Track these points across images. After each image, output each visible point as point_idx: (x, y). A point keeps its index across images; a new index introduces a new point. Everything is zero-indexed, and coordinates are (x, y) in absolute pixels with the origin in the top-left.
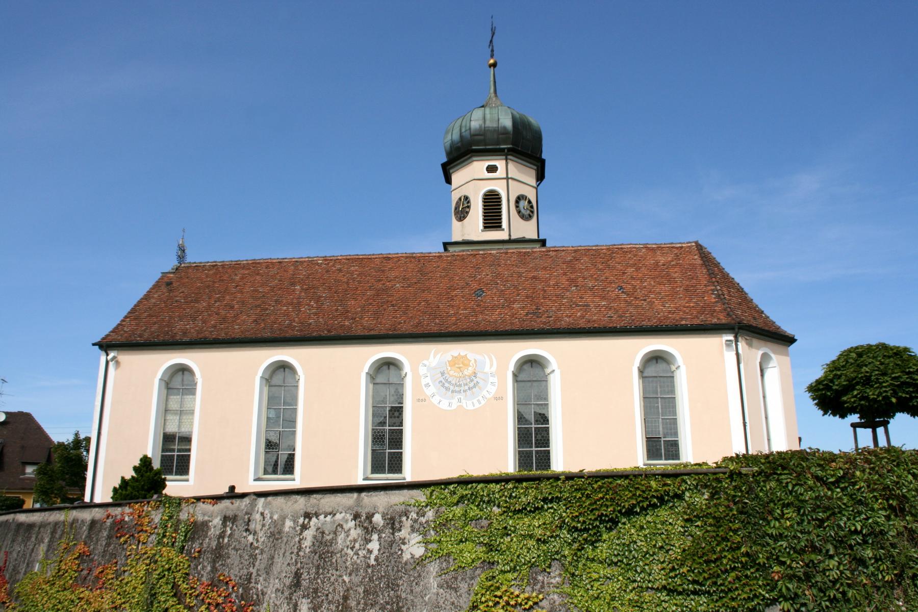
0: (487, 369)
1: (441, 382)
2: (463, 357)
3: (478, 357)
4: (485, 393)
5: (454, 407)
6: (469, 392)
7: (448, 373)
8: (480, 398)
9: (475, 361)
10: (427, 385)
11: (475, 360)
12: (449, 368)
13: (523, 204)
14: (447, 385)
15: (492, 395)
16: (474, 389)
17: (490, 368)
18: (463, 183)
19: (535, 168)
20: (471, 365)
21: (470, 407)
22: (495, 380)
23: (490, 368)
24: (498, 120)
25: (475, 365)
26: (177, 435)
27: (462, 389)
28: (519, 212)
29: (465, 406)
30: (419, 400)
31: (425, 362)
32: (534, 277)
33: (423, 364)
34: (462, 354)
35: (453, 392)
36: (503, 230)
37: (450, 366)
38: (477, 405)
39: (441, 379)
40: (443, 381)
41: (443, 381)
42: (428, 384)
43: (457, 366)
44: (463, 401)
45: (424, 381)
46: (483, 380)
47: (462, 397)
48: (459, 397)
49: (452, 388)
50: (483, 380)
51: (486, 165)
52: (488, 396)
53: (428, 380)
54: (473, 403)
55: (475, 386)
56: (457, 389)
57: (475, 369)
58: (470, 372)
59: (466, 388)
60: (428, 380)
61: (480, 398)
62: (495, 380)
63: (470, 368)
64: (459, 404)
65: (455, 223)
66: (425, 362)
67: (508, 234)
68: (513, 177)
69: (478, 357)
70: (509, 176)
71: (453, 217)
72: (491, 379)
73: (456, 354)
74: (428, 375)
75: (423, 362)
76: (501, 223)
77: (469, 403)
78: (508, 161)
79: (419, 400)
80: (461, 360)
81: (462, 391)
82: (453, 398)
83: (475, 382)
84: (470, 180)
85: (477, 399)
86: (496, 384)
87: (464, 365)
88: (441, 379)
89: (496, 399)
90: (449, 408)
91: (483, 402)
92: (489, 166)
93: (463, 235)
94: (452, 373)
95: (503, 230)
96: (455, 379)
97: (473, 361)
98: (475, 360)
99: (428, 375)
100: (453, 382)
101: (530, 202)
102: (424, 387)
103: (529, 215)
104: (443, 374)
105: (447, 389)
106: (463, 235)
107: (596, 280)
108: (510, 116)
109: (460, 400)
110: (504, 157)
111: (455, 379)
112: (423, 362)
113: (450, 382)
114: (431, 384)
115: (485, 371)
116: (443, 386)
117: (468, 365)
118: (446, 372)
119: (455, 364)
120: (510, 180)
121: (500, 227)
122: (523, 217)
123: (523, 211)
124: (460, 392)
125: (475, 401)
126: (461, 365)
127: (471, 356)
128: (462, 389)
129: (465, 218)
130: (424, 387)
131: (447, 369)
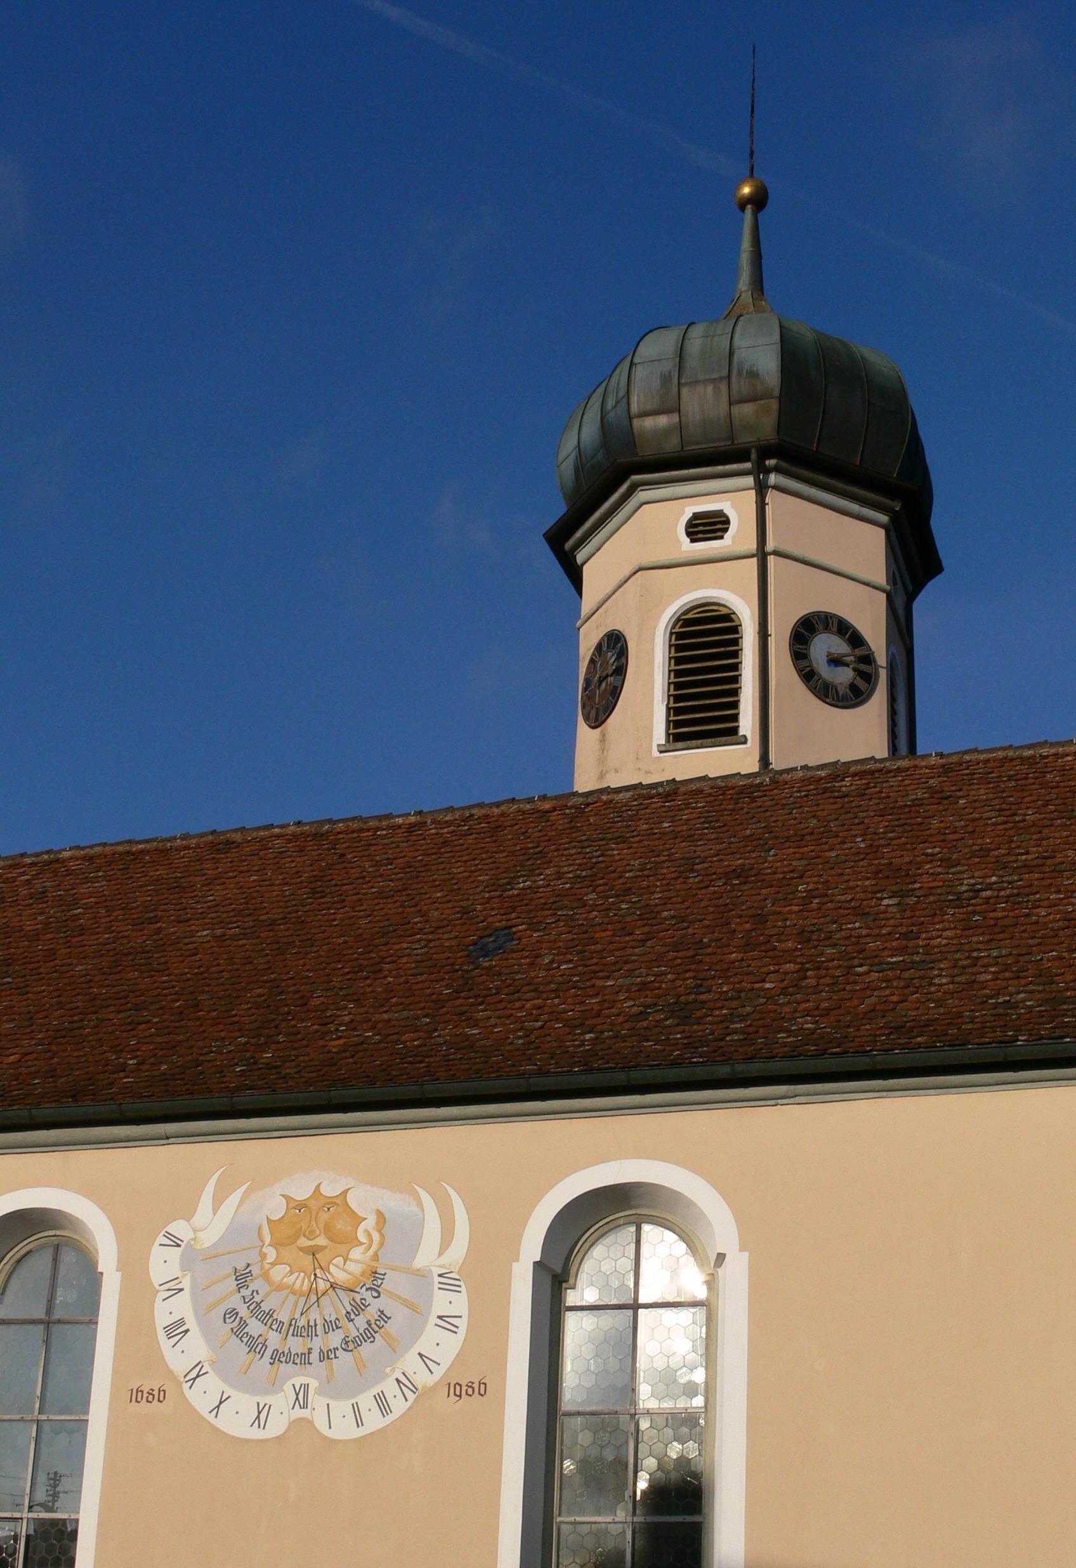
0: (427, 1256)
1: (234, 1313)
2: (330, 1203)
3: (393, 1202)
4: (410, 1363)
5: (276, 1426)
6: (239, 1348)
7: (266, 1276)
8: (390, 1388)
9: (381, 1218)
10: (177, 1329)
11: (380, 1215)
12: (271, 1254)
13: (823, 645)
14: (255, 1327)
15: (439, 1372)
16: (366, 1349)
17: (442, 1251)
18: (610, 589)
19: (884, 518)
20: (362, 1237)
21: (344, 1429)
22: (458, 1304)
23: (442, 1251)
24: (731, 354)
25: (376, 1237)
26: (650, 1519)
27: (317, 1344)
28: (808, 676)
29: (321, 1424)
30: (137, 1395)
31: (179, 1228)
32: (741, 874)
33: (168, 1235)
34: (330, 1190)
35: (277, 1357)
36: (744, 740)
37: (275, 1244)
38: (374, 1421)
39: (236, 1302)
40: (243, 1312)
41: (243, 1312)
42: (181, 1322)
43: (303, 1242)
44: (318, 1402)
45: (164, 1313)
46: (406, 1303)
47: (314, 1384)
48: (298, 1381)
49: (274, 1340)
50: (406, 1303)
51: (688, 515)
52: (423, 1378)
53: (182, 1307)
54: (356, 1408)
55: (369, 1335)
56: (296, 1345)
57: (375, 1257)
58: (355, 1268)
59: (335, 1339)
60: (182, 1307)
61: (390, 1388)
62: (458, 1304)
63: (356, 1253)
64: (298, 1413)
65: (586, 736)
66: (179, 1228)
67: (757, 756)
68: (784, 548)
69: (393, 1202)
70: (770, 546)
71: (580, 718)
72: (442, 1302)
73: (302, 1193)
74: (186, 1283)
75: (167, 1229)
76: (735, 718)
77: (340, 1408)
78: (771, 497)
79: (137, 1395)
80: (324, 1216)
81: (314, 1357)
82: (274, 1386)
83: (372, 1313)
84: (627, 573)
85: (376, 1390)
86: (462, 1324)
87: (331, 1239)
88: (236, 1302)
89: (457, 1390)
90: (256, 1434)
91: (399, 1406)
92: (696, 516)
93: (602, 776)
94: (279, 1273)
95: (744, 740)
96: (292, 1298)
97: (370, 1223)
98: (380, 1215)
99: (186, 1283)
100: (283, 1316)
101: (855, 639)
102: (161, 1335)
103: (853, 687)
104: (242, 1278)
105: (256, 1346)
106: (602, 776)
107: (1001, 865)
108: (776, 337)
109: (302, 1398)
110: (749, 481)
111: (292, 1298)
112: (169, 1229)
113: (270, 1314)
114: (191, 1323)
115: (420, 1262)
116: (240, 1331)
117: (345, 1241)
118: (255, 1269)
119: (296, 1237)
120: (771, 560)
121: (734, 731)
122: (825, 692)
123: (826, 672)
124: (304, 1359)
125: (366, 1401)
126: (321, 1241)
127: (362, 1199)
128: (317, 1344)
129: (609, 709)
130: (161, 1335)
131: (263, 1256)
